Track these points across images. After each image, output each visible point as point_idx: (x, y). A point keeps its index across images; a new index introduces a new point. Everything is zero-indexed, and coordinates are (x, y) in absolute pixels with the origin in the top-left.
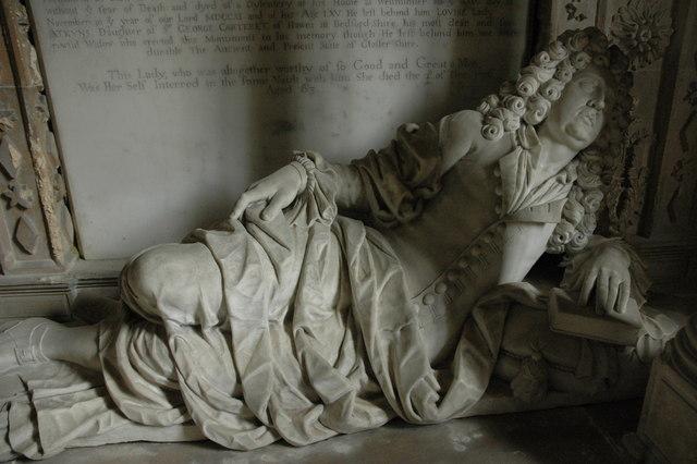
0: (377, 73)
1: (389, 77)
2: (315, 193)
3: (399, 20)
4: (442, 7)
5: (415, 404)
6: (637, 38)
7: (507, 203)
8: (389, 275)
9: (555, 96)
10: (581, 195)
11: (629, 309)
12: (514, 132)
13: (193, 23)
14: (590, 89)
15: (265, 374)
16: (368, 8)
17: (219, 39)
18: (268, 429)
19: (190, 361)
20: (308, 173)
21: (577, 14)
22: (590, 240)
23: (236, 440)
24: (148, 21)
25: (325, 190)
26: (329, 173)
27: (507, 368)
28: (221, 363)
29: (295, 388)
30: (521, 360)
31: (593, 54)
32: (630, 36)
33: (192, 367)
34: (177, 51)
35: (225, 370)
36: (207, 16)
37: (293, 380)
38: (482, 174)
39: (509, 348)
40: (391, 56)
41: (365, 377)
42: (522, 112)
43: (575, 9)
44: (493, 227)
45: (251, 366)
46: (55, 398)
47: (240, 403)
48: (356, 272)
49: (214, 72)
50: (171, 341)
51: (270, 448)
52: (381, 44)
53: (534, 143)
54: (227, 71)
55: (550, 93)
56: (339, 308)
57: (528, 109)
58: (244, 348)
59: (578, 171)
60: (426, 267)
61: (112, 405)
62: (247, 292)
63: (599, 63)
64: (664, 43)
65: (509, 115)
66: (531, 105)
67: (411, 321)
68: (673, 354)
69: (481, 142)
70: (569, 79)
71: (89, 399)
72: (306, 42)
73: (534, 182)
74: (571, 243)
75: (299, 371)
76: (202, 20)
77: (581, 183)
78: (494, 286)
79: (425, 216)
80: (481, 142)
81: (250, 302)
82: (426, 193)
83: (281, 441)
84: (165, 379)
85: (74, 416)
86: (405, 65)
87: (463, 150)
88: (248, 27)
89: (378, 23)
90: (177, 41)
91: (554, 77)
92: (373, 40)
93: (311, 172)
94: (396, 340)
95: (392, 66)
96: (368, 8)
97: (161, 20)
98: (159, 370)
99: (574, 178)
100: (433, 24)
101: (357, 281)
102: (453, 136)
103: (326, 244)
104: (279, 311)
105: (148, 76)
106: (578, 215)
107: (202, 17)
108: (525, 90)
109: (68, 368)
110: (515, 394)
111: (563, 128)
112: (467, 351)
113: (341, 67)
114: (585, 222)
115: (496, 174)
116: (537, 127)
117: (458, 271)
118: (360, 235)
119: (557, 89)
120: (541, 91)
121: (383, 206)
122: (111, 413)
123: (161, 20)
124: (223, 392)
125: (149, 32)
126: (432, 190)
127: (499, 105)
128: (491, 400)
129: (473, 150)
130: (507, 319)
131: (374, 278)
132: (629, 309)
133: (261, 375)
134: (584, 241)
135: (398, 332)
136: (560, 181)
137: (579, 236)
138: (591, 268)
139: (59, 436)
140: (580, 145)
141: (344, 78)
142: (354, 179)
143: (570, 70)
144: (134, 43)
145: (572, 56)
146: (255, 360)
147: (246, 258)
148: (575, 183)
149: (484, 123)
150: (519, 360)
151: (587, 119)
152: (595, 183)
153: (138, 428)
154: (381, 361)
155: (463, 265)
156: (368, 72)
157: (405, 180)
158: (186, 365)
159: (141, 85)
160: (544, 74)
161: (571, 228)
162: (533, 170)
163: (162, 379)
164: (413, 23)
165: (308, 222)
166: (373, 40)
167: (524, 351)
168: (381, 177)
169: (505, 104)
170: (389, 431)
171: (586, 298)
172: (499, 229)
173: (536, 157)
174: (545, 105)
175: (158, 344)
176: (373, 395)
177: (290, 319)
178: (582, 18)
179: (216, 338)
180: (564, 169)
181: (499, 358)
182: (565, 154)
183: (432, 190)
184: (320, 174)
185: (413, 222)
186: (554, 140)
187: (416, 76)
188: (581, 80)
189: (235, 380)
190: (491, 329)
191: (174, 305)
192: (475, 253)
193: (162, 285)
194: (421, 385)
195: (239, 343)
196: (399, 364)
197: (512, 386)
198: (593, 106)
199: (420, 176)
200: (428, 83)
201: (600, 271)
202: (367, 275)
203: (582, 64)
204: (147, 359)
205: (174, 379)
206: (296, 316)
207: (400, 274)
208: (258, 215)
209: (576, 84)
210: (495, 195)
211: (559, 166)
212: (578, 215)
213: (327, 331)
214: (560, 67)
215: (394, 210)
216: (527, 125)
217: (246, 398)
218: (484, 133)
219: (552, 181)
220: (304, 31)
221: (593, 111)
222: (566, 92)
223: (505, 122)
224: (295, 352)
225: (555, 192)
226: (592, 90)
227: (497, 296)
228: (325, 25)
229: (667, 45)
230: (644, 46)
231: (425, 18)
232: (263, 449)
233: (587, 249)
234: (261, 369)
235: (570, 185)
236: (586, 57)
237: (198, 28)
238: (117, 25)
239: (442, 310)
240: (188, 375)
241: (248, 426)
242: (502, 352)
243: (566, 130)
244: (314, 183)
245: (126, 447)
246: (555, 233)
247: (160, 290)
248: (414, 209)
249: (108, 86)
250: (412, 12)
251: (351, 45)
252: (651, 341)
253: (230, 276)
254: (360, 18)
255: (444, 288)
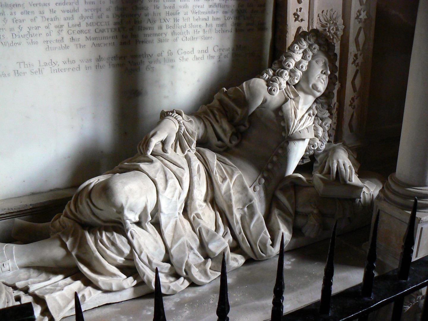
0: (191, 56)
1: (197, 59)
2: (184, 134)
3: (203, 24)
4: (228, 15)
5: (262, 248)
6: (329, 31)
7: (289, 130)
8: (235, 177)
9: (304, 69)
10: (321, 122)
11: (355, 180)
12: (284, 90)
13: (77, 28)
14: (321, 64)
15: (183, 244)
16: (186, 17)
17: (95, 39)
18: (185, 278)
19: (142, 244)
20: (179, 122)
21: (300, 19)
22: (326, 146)
23: (172, 287)
24: (47, 27)
25: (190, 132)
26: (190, 121)
27: (300, 221)
28: (157, 242)
29: (196, 251)
30: (307, 216)
31: (320, 45)
32: (326, 30)
33: (143, 247)
34: (67, 47)
35: (160, 246)
36: (87, 23)
37: (195, 245)
38: (273, 115)
39: (300, 210)
40: (199, 45)
41: (231, 238)
42: (287, 78)
43: (298, 16)
44: (282, 144)
45: (174, 242)
46: (48, 287)
47: (169, 265)
48: (217, 177)
49: (90, 60)
50: (129, 234)
51: (187, 290)
52: (193, 39)
53: (296, 95)
54: (99, 59)
55: (302, 67)
56: (208, 201)
57: (290, 76)
58: (168, 232)
59: (317, 108)
60: (252, 171)
61: (88, 282)
62: (169, 196)
63: (322, 49)
64: (340, 33)
65: (281, 80)
66: (292, 74)
67: (253, 201)
68: (383, 196)
69: (269, 97)
70: (310, 59)
71: (70, 284)
72: (149, 39)
73: (299, 117)
74: (318, 149)
75: (198, 240)
76: (84, 27)
77: (319, 115)
78: (283, 178)
79: (245, 142)
80: (269, 97)
81: (171, 202)
82: (243, 128)
83: (193, 284)
84: (123, 259)
85: (67, 296)
86: (206, 51)
87: (260, 102)
88: (113, 30)
89: (192, 26)
90: (67, 41)
91: (302, 58)
92: (189, 36)
93: (181, 122)
94: (245, 213)
95: (199, 52)
96: (186, 17)
97: (56, 27)
98: (120, 252)
99: (316, 112)
100: (222, 25)
101: (220, 183)
102: (254, 94)
103: (196, 163)
104: (181, 205)
105: (46, 64)
106: (320, 133)
107: (83, 24)
108: (289, 66)
109: (36, 271)
110: (307, 234)
111: (311, 86)
112: (279, 215)
113: (170, 53)
114: (324, 137)
115: (280, 114)
116: (295, 86)
117: (268, 170)
118: (214, 157)
119: (305, 64)
120: (297, 65)
121: (219, 138)
122: (89, 288)
123: (56, 27)
124: (158, 259)
125: (47, 35)
126: (244, 126)
127: (274, 75)
128: (294, 240)
129: (265, 101)
130: (295, 195)
131: (228, 180)
132: (355, 180)
133: (180, 245)
134: (324, 147)
135: (246, 209)
136: (309, 115)
137: (321, 146)
138: (333, 160)
139: (61, 309)
140: (318, 94)
141: (172, 61)
142: (201, 123)
143: (311, 54)
144: (37, 43)
145: (310, 46)
146: (176, 238)
147: (166, 176)
148: (316, 116)
149: (268, 85)
150: (306, 215)
151: (322, 81)
152: (327, 114)
153: (110, 295)
154: (238, 228)
155: (270, 167)
156: (185, 56)
157: (231, 121)
158: (140, 247)
159: (40, 71)
160: (298, 57)
161: (317, 140)
162: (297, 110)
163: (120, 260)
164: (211, 25)
165: (183, 152)
166: (189, 36)
167: (309, 209)
168: (217, 121)
169: (280, 75)
170: (245, 267)
171: (335, 176)
172: (285, 144)
173: (297, 102)
174: (299, 73)
175: (119, 237)
176: (236, 248)
177: (185, 212)
178: (302, 20)
179: (150, 227)
180: (310, 108)
181: (295, 216)
182: (311, 99)
183: (244, 126)
184: (186, 123)
185: (237, 146)
186: (306, 93)
187: (213, 57)
188: (317, 59)
189: (164, 251)
190: (289, 200)
191: (132, 210)
192: (275, 159)
193: (127, 198)
194: (263, 236)
195: (165, 228)
196: (249, 226)
197: (304, 230)
198: (325, 73)
199: (238, 118)
200: (219, 61)
201: (338, 162)
202: (224, 179)
203: (316, 50)
204: (113, 248)
205: (130, 258)
206: (188, 209)
207: (240, 176)
208: (161, 150)
209: (314, 62)
210: (281, 126)
211: (307, 107)
212: (320, 133)
213: (207, 215)
214: (305, 52)
215: (226, 140)
216: (289, 85)
217: (174, 261)
218: (270, 92)
219: (307, 115)
220: (90, 21)
221: (324, 76)
222: (310, 66)
223: (280, 84)
224: (194, 229)
225: (308, 122)
226: (322, 64)
227: (287, 182)
228: (160, 28)
229: (342, 34)
230: (332, 36)
231: (218, 22)
232: (183, 291)
233: (325, 151)
234: (180, 242)
235: (313, 117)
236: (316, 46)
237: (81, 32)
238: (25, 31)
239: (263, 194)
240: (141, 252)
241: (172, 279)
242: (296, 213)
243: (312, 86)
244: (183, 128)
245: (97, 310)
246: (309, 144)
247: (127, 201)
248: (238, 138)
249: (17, 73)
250: (210, 19)
251: (176, 40)
252: (366, 195)
253: (161, 187)
254: (181, 23)
255: (263, 181)
